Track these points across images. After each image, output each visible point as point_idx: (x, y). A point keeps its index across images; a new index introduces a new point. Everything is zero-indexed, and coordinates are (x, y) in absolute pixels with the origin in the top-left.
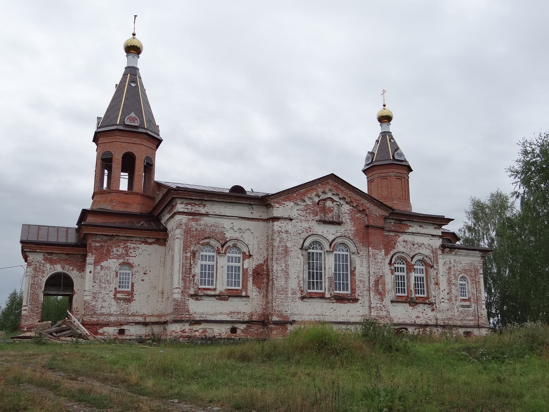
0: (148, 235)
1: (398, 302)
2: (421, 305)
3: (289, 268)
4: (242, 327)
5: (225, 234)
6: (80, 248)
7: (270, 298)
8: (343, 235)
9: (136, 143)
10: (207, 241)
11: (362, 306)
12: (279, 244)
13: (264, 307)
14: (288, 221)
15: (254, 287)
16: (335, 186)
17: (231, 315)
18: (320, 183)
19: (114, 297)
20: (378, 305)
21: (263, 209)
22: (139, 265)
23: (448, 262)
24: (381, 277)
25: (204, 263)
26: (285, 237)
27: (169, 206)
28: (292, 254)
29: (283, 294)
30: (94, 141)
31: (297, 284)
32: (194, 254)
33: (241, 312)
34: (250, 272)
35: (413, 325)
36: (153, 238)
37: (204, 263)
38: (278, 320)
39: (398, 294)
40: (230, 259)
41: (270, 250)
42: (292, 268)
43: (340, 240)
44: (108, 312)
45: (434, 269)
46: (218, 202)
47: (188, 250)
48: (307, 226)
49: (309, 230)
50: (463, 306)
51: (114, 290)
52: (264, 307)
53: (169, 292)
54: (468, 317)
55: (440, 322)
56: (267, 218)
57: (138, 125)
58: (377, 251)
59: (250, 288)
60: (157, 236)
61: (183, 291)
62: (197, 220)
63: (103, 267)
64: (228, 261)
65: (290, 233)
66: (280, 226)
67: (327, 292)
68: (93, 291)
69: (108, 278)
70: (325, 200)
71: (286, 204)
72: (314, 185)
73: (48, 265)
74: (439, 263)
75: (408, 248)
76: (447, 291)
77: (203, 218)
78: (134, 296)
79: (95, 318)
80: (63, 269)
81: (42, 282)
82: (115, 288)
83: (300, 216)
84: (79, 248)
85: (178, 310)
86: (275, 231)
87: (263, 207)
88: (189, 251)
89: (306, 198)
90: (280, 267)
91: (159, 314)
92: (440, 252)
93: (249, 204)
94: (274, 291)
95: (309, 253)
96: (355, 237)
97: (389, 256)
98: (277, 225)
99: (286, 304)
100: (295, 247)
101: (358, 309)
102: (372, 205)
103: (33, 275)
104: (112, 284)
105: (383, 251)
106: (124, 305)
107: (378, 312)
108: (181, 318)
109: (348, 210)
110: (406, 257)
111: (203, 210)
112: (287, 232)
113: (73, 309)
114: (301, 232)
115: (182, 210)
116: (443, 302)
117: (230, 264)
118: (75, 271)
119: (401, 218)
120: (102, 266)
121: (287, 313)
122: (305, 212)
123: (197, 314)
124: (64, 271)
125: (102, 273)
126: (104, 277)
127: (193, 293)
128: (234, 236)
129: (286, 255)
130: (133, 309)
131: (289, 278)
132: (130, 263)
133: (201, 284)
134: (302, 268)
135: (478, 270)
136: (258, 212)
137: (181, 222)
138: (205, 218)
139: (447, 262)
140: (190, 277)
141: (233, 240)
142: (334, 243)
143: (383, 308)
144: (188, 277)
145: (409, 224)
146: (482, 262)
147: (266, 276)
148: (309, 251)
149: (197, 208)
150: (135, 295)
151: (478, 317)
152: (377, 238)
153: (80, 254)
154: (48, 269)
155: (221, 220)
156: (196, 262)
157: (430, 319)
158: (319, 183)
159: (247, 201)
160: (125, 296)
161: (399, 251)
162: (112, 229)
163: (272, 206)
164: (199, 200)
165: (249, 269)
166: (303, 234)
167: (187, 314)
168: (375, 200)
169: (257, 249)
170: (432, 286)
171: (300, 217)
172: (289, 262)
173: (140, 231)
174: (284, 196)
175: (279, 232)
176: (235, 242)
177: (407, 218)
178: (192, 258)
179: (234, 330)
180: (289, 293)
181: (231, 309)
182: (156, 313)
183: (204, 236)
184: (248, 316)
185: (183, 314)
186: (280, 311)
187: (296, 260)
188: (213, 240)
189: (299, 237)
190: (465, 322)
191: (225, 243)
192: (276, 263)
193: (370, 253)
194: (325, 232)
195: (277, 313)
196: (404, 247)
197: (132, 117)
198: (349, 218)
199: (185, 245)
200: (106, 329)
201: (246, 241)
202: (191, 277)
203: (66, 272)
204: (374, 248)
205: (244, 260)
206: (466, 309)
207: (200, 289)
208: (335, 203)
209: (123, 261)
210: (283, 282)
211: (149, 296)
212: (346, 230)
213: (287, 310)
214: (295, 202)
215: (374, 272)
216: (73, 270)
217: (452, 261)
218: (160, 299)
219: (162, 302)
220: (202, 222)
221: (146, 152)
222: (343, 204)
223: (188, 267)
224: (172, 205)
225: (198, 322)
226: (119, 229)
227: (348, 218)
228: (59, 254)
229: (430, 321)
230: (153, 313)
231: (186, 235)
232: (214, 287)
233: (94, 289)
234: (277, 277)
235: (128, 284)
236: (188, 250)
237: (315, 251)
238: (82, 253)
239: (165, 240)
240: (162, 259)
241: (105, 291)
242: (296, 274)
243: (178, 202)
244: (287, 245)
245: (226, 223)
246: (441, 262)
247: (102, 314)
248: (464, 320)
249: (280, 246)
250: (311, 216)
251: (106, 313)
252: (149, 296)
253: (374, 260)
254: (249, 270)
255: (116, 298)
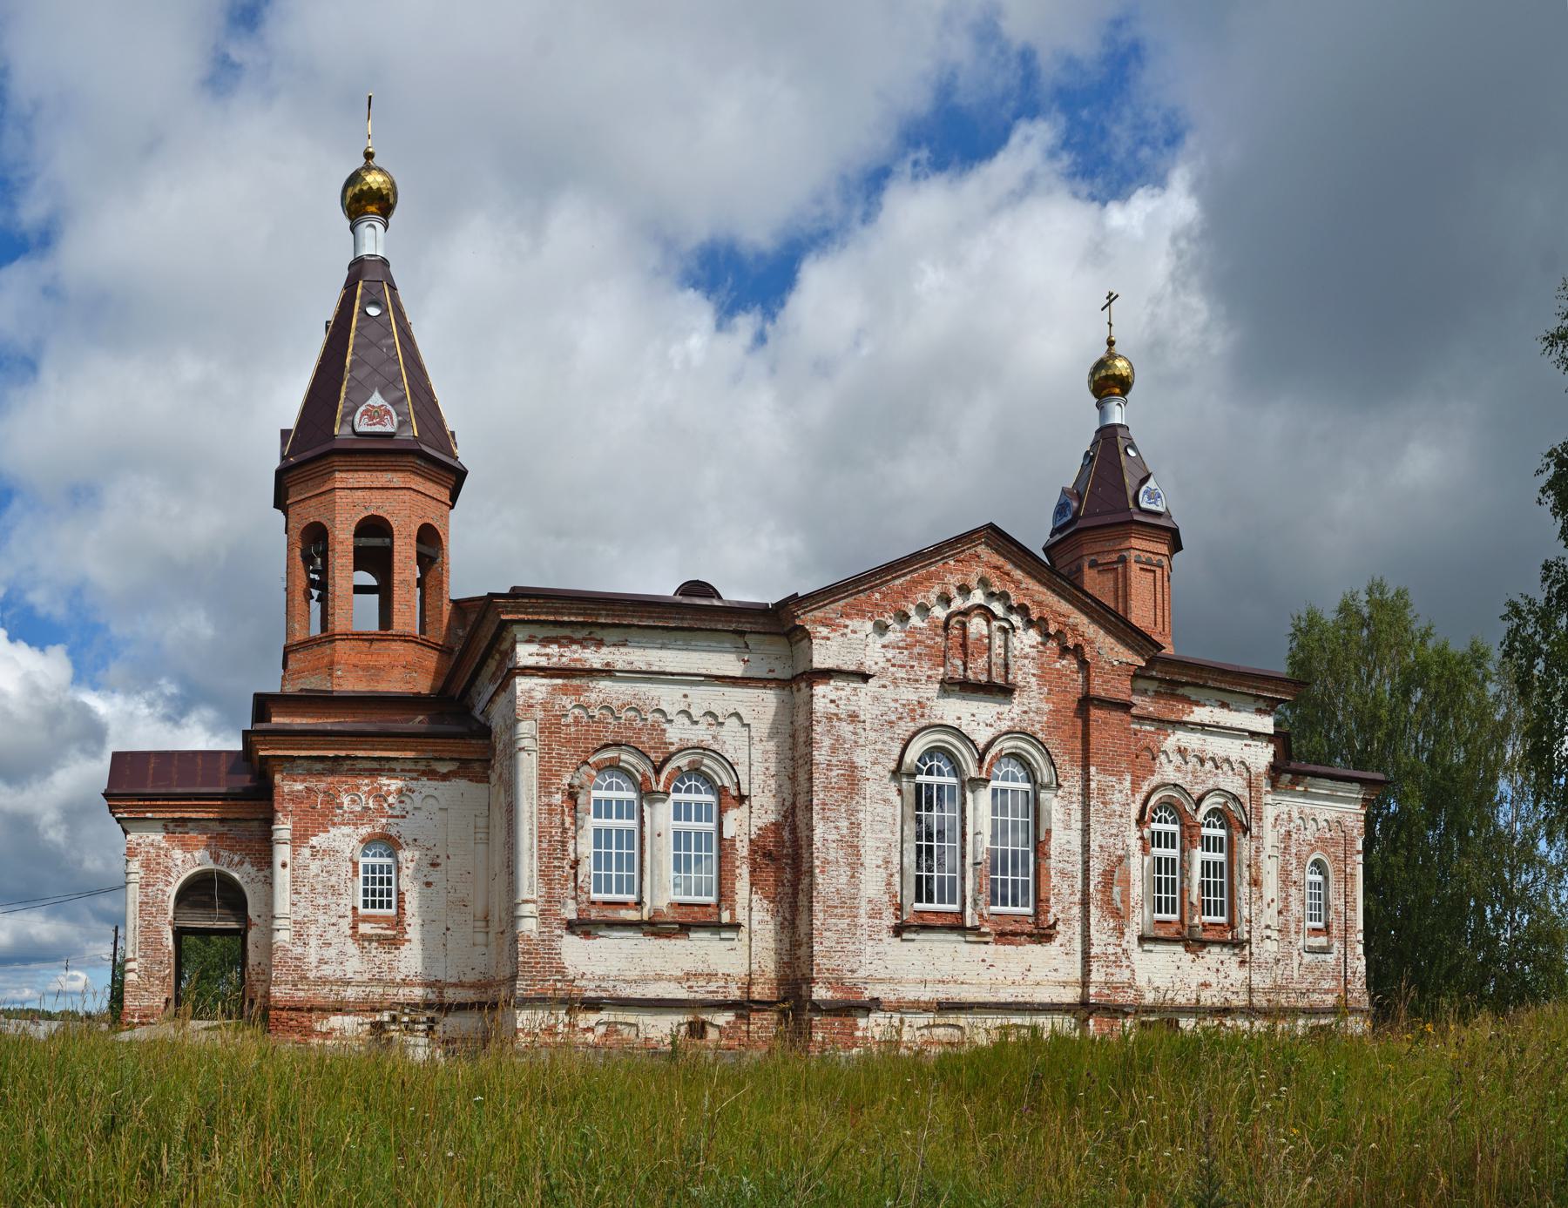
0: (436, 751)
1: (1156, 940)
2: (1216, 949)
3: (862, 834)
4: (724, 1018)
5: (664, 730)
6: (257, 803)
7: (803, 929)
8: (1017, 729)
9: (391, 485)
10: (611, 755)
11: (1067, 954)
12: (829, 758)
13: (785, 957)
14: (858, 682)
15: (755, 897)
16: (997, 568)
17: (690, 983)
18: (952, 555)
19: (350, 932)
20: (1111, 950)
21: (779, 646)
22: (415, 840)
23: (1286, 816)
24: (1121, 859)
25: (604, 823)
26: (849, 736)
27: (493, 658)
28: (870, 788)
29: (843, 916)
30: (276, 506)
31: (884, 884)
32: (572, 795)
33: (716, 975)
34: (743, 850)
35: (1196, 1010)
36: (452, 759)
37: (604, 823)
38: (829, 998)
39: (1158, 916)
40: (681, 811)
41: (802, 777)
42: (868, 835)
43: (1007, 745)
44: (339, 974)
45: (1251, 837)
46: (641, 631)
47: (553, 784)
48: (914, 697)
49: (919, 712)
50: (1312, 950)
51: (349, 913)
52: (785, 957)
53: (503, 914)
54: (1323, 982)
55: (1260, 1001)
56: (789, 677)
57: (393, 430)
58: (1110, 778)
59: (742, 901)
60: (460, 752)
61: (546, 910)
62: (578, 691)
63: (318, 851)
64: (677, 817)
65: (864, 722)
66: (833, 697)
67: (969, 911)
68: (293, 917)
69: (334, 879)
70: (965, 613)
71: (851, 628)
72: (937, 561)
73: (177, 851)
74: (1264, 818)
75: (1187, 773)
76: (1275, 907)
77: (595, 683)
78: (408, 929)
79: (303, 990)
80: (216, 860)
81: (165, 898)
82: (355, 909)
83: (893, 665)
84: (250, 803)
85: (533, 967)
86: (818, 715)
87: (776, 638)
88: (558, 789)
89: (911, 606)
90: (834, 831)
91: (480, 981)
92: (1265, 786)
93: (735, 632)
94: (817, 907)
95: (918, 787)
96: (1050, 734)
97: (1140, 798)
98: (824, 697)
99: (852, 948)
100: (878, 768)
101: (1055, 964)
102: (1102, 632)
103: (143, 880)
104: (344, 896)
105: (1128, 778)
106: (380, 955)
107: (1109, 970)
108: (540, 991)
109: (1033, 647)
110: (1182, 800)
111: (594, 658)
112: (853, 717)
113: (250, 968)
114: (893, 718)
115: (531, 661)
116: (1268, 937)
117: (683, 825)
118: (247, 867)
119: (1176, 677)
120: (314, 847)
121: (855, 975)
122: (906, 652)
123: (590, 980)
124: (219, 868)
125: (315, 867)
126: (321, 879)
127: (574, 916)
128: (692, 737)
129: (850, 793)
130: (408, 965)
131: (862, 865)
132: (391, 836)
133: (597, 890)
134: (899, 834)
135: (1353, 840)
136: (763, 656)
137: (532, 698)
138: (604, 684)
139: (1282, 816)
140: (563, 867)
141: (688, 749)
142: (994, 751)
143: (1124, 959)
144: (559, 867)
145: (1194, 698)
146: (1363, 818)
147: (789, 861)
148: (921, 778)
149: (575, 652)
150: (409, 925)
151: (1345, 980)
152: (1113, 737)
153: (257, 819)
154: (179, 862)
155: (650, 685)
156: (580, 823)
157: (1234, 989)
158: (949, 556)
159: (731, 622)
160: (382, 928)
161: (1166, 781)
162: (333, 738)
163: (808, 636)
164: (583, 625)
165: (738, 839)
166: (902, 723)
167: (559, 981)
168: (1111, 614)
169: (763, 777)
170: (1244, 890)
171: (891, 669)
172: (861, 815)
173: (412, 740)
174: (846, 601)
175: (830, 719)
176: (697, 757)
177: (1191, 676)
178: (566, 810)
179: (698, 1029)
180: (862, 912)
181: (689, 965)
182: (471, 977)
183: (600, 740)
184: (740, 985)
185: (549, 980)
186: (833, 970)
187: (880, 808)
188: (629, 752)
189: (889, 735)
190: (1316, 996)
191: (666, 761)
192: (823, 818)
193: (1093, 785)
194: (966, 718)
195: (827, 975)
196: (1178, 769)
197: (373, 407)
198: (1035, 672)
199: (546, 770)
200: (336, 1021)
201: (727, 751)
202: (567, 868)
203: (224, 869)
204: (1103, 770)
205: (721, 812)
206: (1321, 957)
207: (593, 903)
208: (995, 624)
209: (369, 830)
210: (844, 879)
211: (448, 929)
212: (1025, 712)
213: (855, 967)
214: (877, 618)
215: (1101, 847)
216: (241, 863)
217: (1295, 815)
218: (480, 938)
219: (487, 946)
220: (594, 696)
221: (420, 512)
222: (1019, 628)
223: (556, 838)
224: (501, 653)
225: (594, 1005)
226: (354, 739)
227: (1032, 671)
228: (202, 823)
229: (1234, 997)
230: (462, 977)
231: (547, 737)
232: (633, 898)
233: (295, 912)
234: (826, 862)
235: (389, 895)
236: (553, 784)
237: (934, 779)
238: (261, 816)
239: (487, 763)
240: (481, 822)
241: (326, 917)
242: (880, 853)
243: (519, 636)
244: (855, 759)
245: (668, 697)
246: (1269, 813)
247: (324, 981)
248: (1314, 991)
249: (834, 762)
250: (926, 665)
251: (332, 979)
252: (448, 929)
253: (1101, 806)
254: (738, 845)
255: (355, 935)
